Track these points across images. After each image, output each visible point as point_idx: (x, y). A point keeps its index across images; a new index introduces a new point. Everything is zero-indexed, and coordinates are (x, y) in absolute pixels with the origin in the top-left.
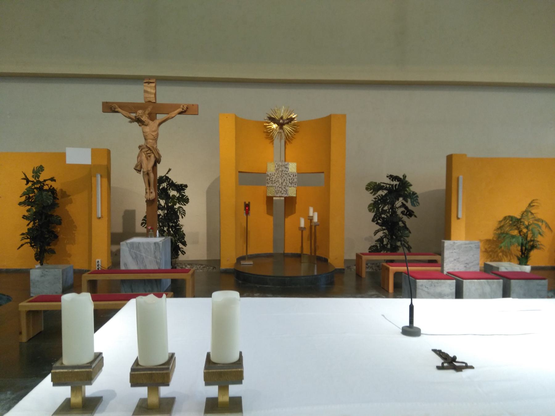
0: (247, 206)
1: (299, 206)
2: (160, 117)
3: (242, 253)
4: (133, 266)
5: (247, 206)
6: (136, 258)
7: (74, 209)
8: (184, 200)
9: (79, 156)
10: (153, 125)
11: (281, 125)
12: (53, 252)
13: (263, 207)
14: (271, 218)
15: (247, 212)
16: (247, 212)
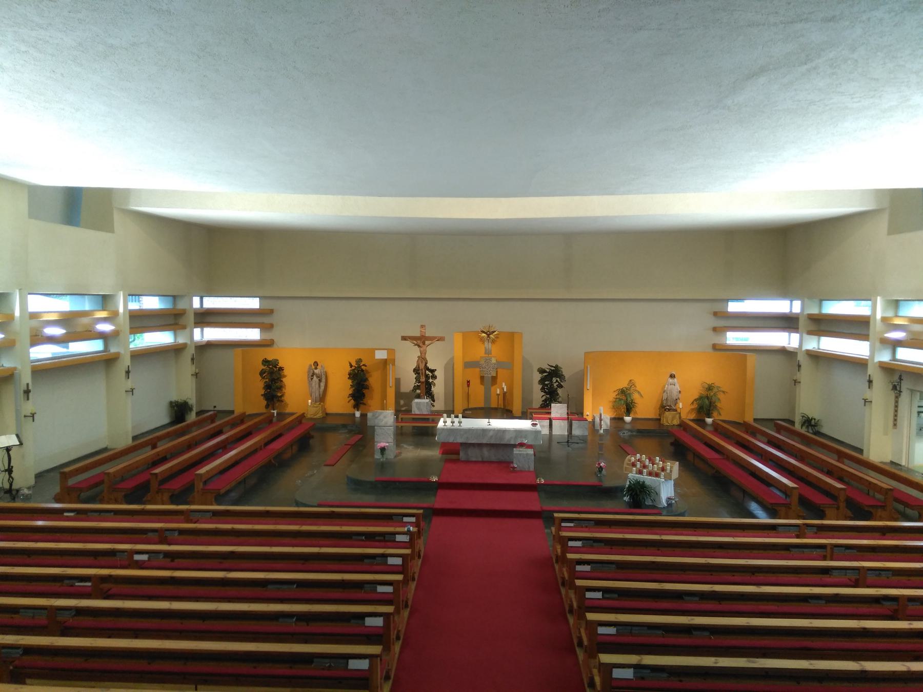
0: (468, 382)
1: (499, 380)
2: (427, 342)
3: (466, 407)
4: (417, 412)
5: (468, 382)
6: (419, 409)
7: (374, 380)
8: (434, 377)
9: (381, 355)
10: (424, 347)
11: (488, 335)
12: (364, 404)
13: (478, 381)
14: (483, 387)
15: (468, 386)
16: (468, 386)
